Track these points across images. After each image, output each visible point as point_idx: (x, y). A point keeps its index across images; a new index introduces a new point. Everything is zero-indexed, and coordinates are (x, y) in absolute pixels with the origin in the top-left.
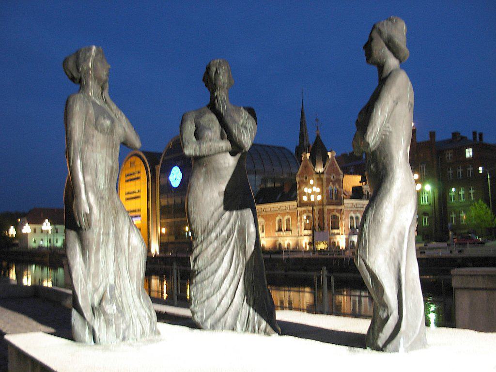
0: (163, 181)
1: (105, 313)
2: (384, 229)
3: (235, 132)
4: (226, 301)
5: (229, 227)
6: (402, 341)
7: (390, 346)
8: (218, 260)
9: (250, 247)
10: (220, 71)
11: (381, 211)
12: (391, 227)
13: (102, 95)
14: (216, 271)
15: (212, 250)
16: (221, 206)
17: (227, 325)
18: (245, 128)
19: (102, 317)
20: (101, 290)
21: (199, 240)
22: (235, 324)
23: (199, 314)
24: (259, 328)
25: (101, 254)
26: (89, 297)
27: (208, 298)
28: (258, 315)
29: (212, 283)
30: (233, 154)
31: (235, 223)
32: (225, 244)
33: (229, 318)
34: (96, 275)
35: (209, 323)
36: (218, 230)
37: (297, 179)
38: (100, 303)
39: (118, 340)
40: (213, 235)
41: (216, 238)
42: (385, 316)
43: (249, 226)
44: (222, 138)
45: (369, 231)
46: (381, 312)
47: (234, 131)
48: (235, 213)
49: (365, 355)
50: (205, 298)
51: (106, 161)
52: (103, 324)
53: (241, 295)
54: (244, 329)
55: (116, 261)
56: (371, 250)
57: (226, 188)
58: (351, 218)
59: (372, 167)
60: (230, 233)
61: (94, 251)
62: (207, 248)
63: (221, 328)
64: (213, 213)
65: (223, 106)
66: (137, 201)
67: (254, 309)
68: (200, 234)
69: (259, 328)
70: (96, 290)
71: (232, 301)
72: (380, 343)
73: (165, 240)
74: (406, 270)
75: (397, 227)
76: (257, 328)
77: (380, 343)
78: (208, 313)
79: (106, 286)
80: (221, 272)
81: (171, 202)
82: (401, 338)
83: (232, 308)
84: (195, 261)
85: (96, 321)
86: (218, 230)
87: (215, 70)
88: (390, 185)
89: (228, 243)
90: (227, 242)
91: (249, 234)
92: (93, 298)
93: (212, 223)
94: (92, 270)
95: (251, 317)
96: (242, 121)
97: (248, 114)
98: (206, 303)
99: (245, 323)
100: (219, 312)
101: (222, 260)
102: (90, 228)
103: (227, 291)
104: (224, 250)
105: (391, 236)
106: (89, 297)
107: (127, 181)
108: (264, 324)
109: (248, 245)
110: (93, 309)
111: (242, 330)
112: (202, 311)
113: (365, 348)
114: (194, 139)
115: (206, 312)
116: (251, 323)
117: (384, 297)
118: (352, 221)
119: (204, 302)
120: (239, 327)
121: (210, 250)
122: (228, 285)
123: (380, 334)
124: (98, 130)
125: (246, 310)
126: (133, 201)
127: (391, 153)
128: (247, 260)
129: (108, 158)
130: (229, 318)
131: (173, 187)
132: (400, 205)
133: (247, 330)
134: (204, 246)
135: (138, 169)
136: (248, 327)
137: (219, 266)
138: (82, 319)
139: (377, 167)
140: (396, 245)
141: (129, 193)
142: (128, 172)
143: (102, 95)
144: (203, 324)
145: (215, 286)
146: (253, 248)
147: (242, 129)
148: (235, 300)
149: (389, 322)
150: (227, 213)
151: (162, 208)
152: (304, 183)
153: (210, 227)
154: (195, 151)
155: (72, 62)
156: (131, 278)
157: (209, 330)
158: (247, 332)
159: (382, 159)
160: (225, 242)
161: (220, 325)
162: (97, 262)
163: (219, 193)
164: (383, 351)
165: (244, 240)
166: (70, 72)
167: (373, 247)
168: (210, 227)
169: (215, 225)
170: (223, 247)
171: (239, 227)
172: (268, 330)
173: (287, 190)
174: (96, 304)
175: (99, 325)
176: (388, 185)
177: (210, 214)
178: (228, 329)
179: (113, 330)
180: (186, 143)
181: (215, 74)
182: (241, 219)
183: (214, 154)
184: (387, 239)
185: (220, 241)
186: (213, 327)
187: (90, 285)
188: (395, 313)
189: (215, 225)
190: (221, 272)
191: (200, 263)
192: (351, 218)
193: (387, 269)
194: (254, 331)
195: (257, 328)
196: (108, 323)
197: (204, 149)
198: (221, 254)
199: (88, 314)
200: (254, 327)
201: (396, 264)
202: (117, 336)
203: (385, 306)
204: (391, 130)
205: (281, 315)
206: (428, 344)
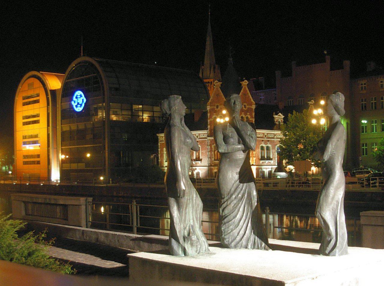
0: (66, 106)
1: (191, 240)
2: (330, 200)
3: (247, 140)
4: (242, 232)
5: (242, 192)
6: (337, 250)
7: (331, 253)
8: (237, 210)
9: (255, 203)
10: (237, 103)
11: (329, 191)
12: (333, 198)
13: (181, 123)
14: (236, 216)
15: (233, 205)
16: (238, 181)
17: (243, 245)
18: (252, 137)
19: (189, 242)
20: (188, 228)
21: (226, 199)
22: (247, 245)
23: (227, 240)
24: (261, 246)
25: (187, 210)
26: (182, 232)
27: (232, 231)
28: (260, 240)
29: (234, 223)
30: (244, 151)
31: (246, 190)
32: (240, 202)
33: (244, 242)
34: (185, 221)
35: (233, 244)
36: (236, 194)
37: (208, 108)
38: (189, 234)
39: (196, 254)
40: (234, 196)
41: (235, 198)
42: (329, 240)
43: (253, 192)
44: (239, 143)
45: (323, 201)
46: (327, 238)
47: (247, 140)
48: (245, 184)
49: (320, 258)
50: (230, 231)
51: (188, 161)
52: (189, 246)
53: (250, 229)
54: (252, 247)
55: (192, 213)
56: (324, 209)
57: (240, 170)
58: (262, 148)
59: (324, 169)
60: (243, 195)
61: (184, 208)
62: (230, 204)
63: (239, 247)
64: (233, 184)
65: (239, 124)
66: (36, 126)
67: (257, 236)
68: (226, 196)
69: (261, 246)
70: (185, 228)
71: (245, 233)
72: (327, 252)
73: (67, 166)
74: (339, 218)
75: (336, 198)
76: (260, 246)
77: (327, 252)
78: (232, 239)
79: (189, 226)
80: (238, 216)
81: (74, 127)
82: (337, 250)
83: (245, 236)
84: (223, 210)
85: (185, 244)
86: (236, 194)
87: (233, 101)
88: (333, 179)
89: (242, 201)
90: (241, 200)
91: (253, 197)
92: (184, 232)
93: (233, 189)
94: (183, 218)
95: (256, 241)
96: (249, 132)
97: (252, 128)
98: (231, 233)
99: (253, 245)
100: (238, 238)
101: (239, 210)
102: (184, 197)
103: (242, 227)
104: (240, 205)
105: (333, 203)
106: (182, 232)
107: (24, 104)
108: (263, 244)
109: (253, 202)
110: (184, 238)
111: (251, 248)
112: (229, 238)
113: (319, 254)
114: (224, 143)
115: (231, 238)
116: (256, 244)
117: (329, 231)
118: (263, 151)
119: (230, 233)
120: (249, 246)
121: (232, 205)
122: (242, 224)
123: (327, 248)
124: (185, 145)
125: (253, 236)
126: (31, 126)
127: (334, 164)
128: (253, 210)
129: (189, 159)
130: (244, 242)
131: (76, 112)
132: (337, 188)
133: (254, 248)
134: (229, 202)
135: (37, 92)
136: (255, 246)
137: (237, 214)
138: (178, 243)
139: (327, 169)
140: (335, 207)
141: (29, 117)
142: (25, 95)
143: (181, 123)
144: (229, 245)
145: (235, 225)
146: (256, 204)
147: (251, 139)
148: (247, 232)
149: (332, 242)
150: (241, 184)
151: (63, 133)
152: (215, 112)
153: (232, 192)
154: (225, 150)
155: (166, 105)
156: (197, 221)
157: (233, 248)
158: (254, 249)
159: (330, 166)
160: (240, 200)
161: (239, 245)
162: (186, 213)
163: (236, 173)
164: (328, 256)
165: (251, 199)
166: (165, 110)
167: (325, 208)
168: (232, 192)
169: (235, 191)
170: (239, 204)
171: (248, 192)
172: (266, 247)
173: (197, 118)
174: (186, 234)
175: (187, 246)
176: (332, 179)
177: (231, 185)
178: (244, 248)
179: (195, 249)
180: (220, 146)
181: (234, 104)
182: (249, 188)
183: (236, 151)
184: (331, 204)
185: (237, 200)
186: (235, 247)
187: (182, 226)
188: (334, 238)
189: (235, 191)
190: (238, 216)
191: (226, 212)
192: (262, 148)
193: (331, 218)
194: (258, 248)
195: (260, 246)
196: (192, 245)
197: (230, 148)
198: (238, 207)
199: (181, 240)
200: (258, 246)
201: (335, 216)
202: (196, 252)
203: (330, 235)
204: (335, 152)
205: (271, 241)
206: (349, 253)
